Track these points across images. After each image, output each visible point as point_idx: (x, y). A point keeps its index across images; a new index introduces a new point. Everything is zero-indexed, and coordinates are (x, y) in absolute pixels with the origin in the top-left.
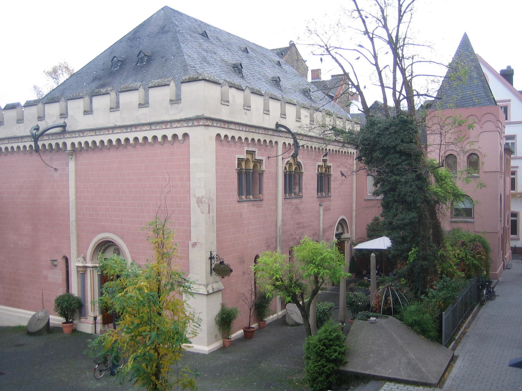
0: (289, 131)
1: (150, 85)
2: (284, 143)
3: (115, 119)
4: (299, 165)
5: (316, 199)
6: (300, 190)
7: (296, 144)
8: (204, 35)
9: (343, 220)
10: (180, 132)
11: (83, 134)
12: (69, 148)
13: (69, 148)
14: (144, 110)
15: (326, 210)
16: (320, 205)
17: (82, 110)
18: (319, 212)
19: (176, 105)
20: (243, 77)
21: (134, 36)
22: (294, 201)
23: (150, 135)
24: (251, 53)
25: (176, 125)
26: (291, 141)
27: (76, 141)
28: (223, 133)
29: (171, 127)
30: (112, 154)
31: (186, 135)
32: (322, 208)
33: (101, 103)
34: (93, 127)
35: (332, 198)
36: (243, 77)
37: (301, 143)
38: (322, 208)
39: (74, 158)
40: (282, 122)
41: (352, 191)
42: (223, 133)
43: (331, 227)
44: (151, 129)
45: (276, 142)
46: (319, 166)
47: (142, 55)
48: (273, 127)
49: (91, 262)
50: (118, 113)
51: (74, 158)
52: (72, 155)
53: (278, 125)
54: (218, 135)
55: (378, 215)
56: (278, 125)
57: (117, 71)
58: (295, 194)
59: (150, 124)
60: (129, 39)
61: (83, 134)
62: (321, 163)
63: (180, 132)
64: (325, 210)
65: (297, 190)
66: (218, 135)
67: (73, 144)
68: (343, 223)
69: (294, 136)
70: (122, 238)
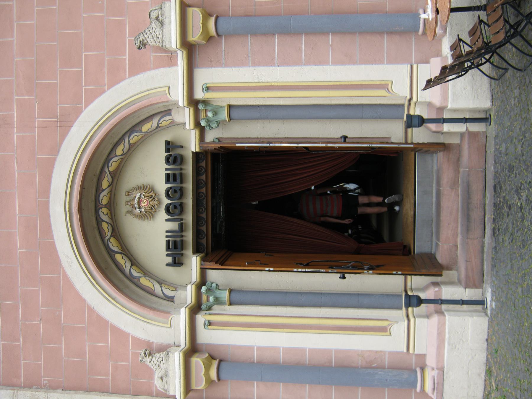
49: (174, 318)
70: (64, 125)
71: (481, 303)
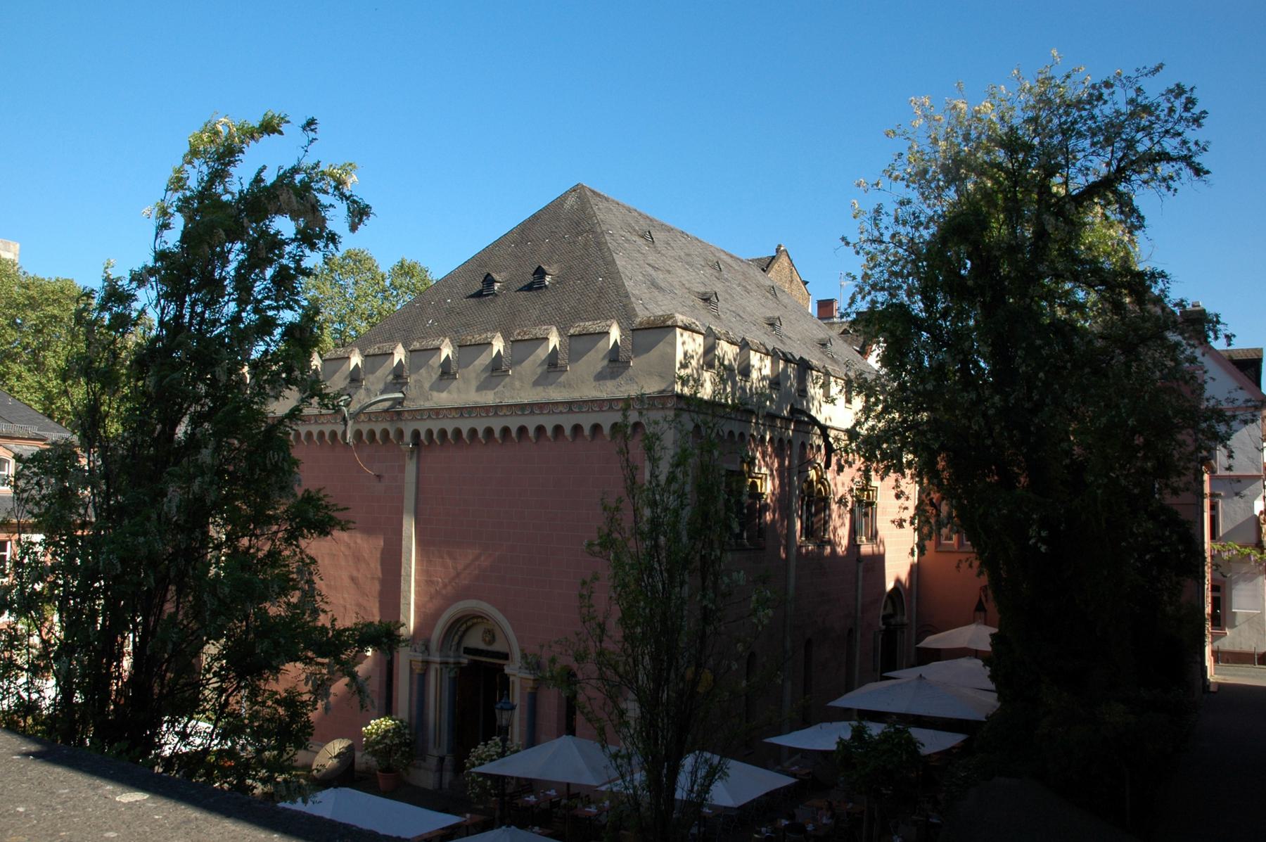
24: (725, 273)
67: (416, 434)
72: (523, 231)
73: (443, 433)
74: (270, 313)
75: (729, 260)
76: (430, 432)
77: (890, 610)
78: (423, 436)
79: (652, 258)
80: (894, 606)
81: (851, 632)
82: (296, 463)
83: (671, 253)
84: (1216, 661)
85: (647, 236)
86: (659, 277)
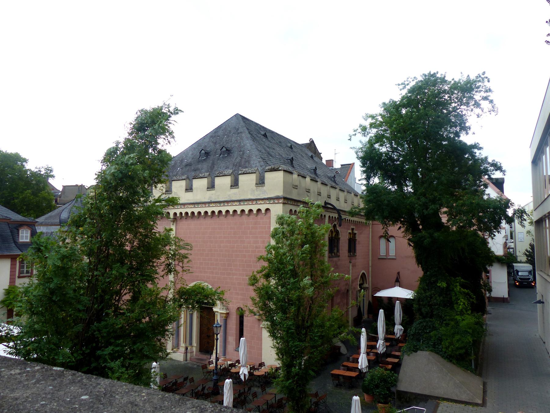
0: (334, 208)
1: (240, 172)
2: (329, 216)
3: (235, 194)
4: (337, 232)
5: (347, 257)
6: (338, 251)
7: (340, 216)
8: (265, 135)
9: (363, 273)
10: (263, 207)
11: (184, 206)
12: (172, 216)
13: (172, 216)
14: (235, 191)
15: (354, 266)
16: (350, 262)
17: (184, 188)
18: (349, 268)
19: (260, 188)
20: (293, 167)
21: (215, 135)
22: (335, 259)
23: (202, 211)
24: (294, 149)
25: (261, 202)
26: (336, 216)
27: (178, 211)
28: (294, 208)
29: (256, 204)
30: (209, 221)
31: (267, 210)
32: (351, 265)
33: (200, 184)
34: (192, 202)
35: (357, 257)
36: (293, 167)
37: (343, 217)
38: (351, 265)
39: (175, 224)
40: (329, 201)
41: (369, 252)
42: (294, 208)
43: (357, 278)
44: (240, 205)
45: (325, 216)
46: (349, 233)
47: (224, 149)
48: (323, 204)
50: (213, 192)
51: (175, 224)
52: (174, 222)
53: (326, 203)
54: (291, 210)
55: (486, 190)
56: (326, 203)
57: (204, 160)
58: (334, 253)
59: (240, 201)
60: (211, 137)
61: (184, 206)
62: (350, 231)
63: (263, 207)
64: (353, 266)
65: (335, 251)
66: (291, 210)
67: (175, 214)
68: (363, 276)
69: (339, 211)
71: (186, 361)
72: (215, 132)
73: (187, 213)
74: (196, 390)
75: (295, 145)
76: (181, 213)
77: (361, 282)
78: (178, 215)
79: (267, 143)
80: (363, 281)
81: (348, 291)
82: (153, 109)
83: (273, 141)
84: (489, 301)
85: (265, 135)
86: (271, 151)
